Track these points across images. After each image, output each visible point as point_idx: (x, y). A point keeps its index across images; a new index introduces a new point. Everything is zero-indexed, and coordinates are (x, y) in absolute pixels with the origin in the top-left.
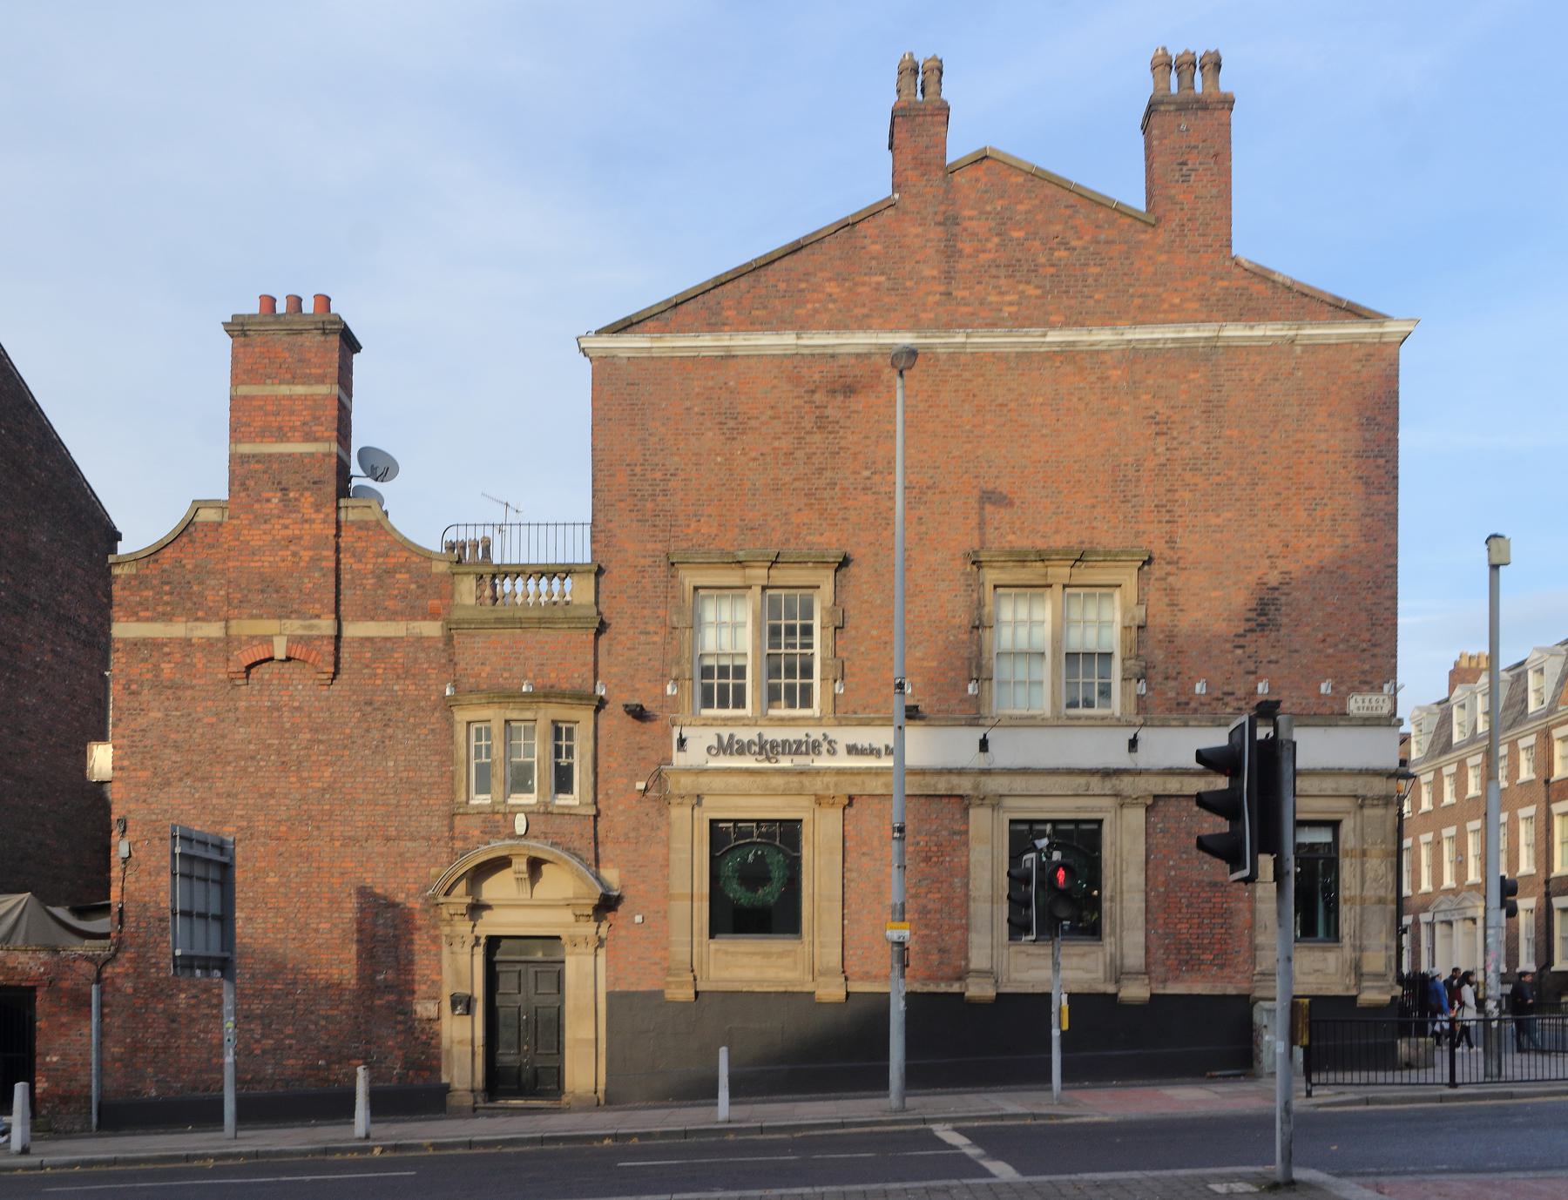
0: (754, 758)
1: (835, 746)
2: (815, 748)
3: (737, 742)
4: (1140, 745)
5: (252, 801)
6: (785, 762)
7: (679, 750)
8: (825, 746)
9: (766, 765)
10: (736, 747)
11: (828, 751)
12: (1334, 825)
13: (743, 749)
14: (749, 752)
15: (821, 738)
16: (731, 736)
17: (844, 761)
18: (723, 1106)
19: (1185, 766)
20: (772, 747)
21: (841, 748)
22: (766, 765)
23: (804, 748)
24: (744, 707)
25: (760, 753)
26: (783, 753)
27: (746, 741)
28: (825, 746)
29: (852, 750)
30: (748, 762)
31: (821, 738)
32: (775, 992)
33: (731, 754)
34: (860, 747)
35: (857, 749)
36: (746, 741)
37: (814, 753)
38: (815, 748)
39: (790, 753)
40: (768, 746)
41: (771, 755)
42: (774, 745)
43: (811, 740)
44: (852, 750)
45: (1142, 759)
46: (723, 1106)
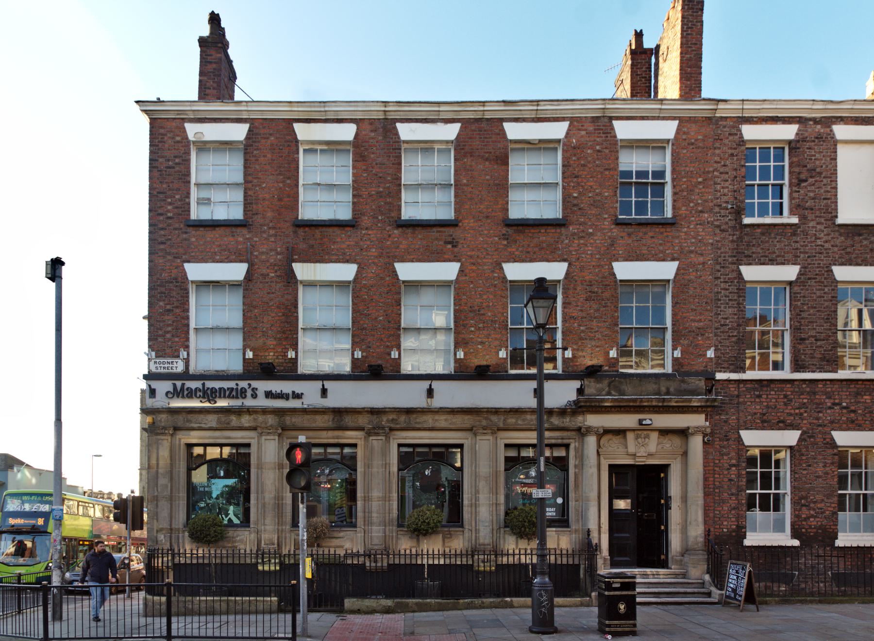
0: (199, 400)
1: (257, 392)
2: (242, 394)
3: (188, 389)
4: (435, 394)
5: (817, 397)
6: (222, 403)
7: (150, 397)
8: (249, 393)
9: (207, 405)
10: (186, 392)
11: (252, 395)
12: (567, 446)
13: (191, 394)
14: (196, 396)
15: (246, 387)
16: (183, 385)
17: (262, 402)
18: (758, 147)
19: (470, 407)
20: (212, 393)
21: (261, 393)
22: (207, 405)
23: (234, 393)
24: (610, 466)
25: (204, 397)
26: (220, 397)
27: (193, 388)
28: (249, 393)
29: (269, 395)
30: (195, 403)
31: (246, 387)
32: (249, 488)
33: (183, 397)
34: (274, 392)
35: (272, 394)
36: (193, 388)
37: (191, 389)
38: (242, 394)
39: (224, 397)
40: (209, 392)
41: (211, 398)
42: (214, 391)
43: (239, 388)
44: (269, 395)
45: (438, 402)
46: (758, 147)
